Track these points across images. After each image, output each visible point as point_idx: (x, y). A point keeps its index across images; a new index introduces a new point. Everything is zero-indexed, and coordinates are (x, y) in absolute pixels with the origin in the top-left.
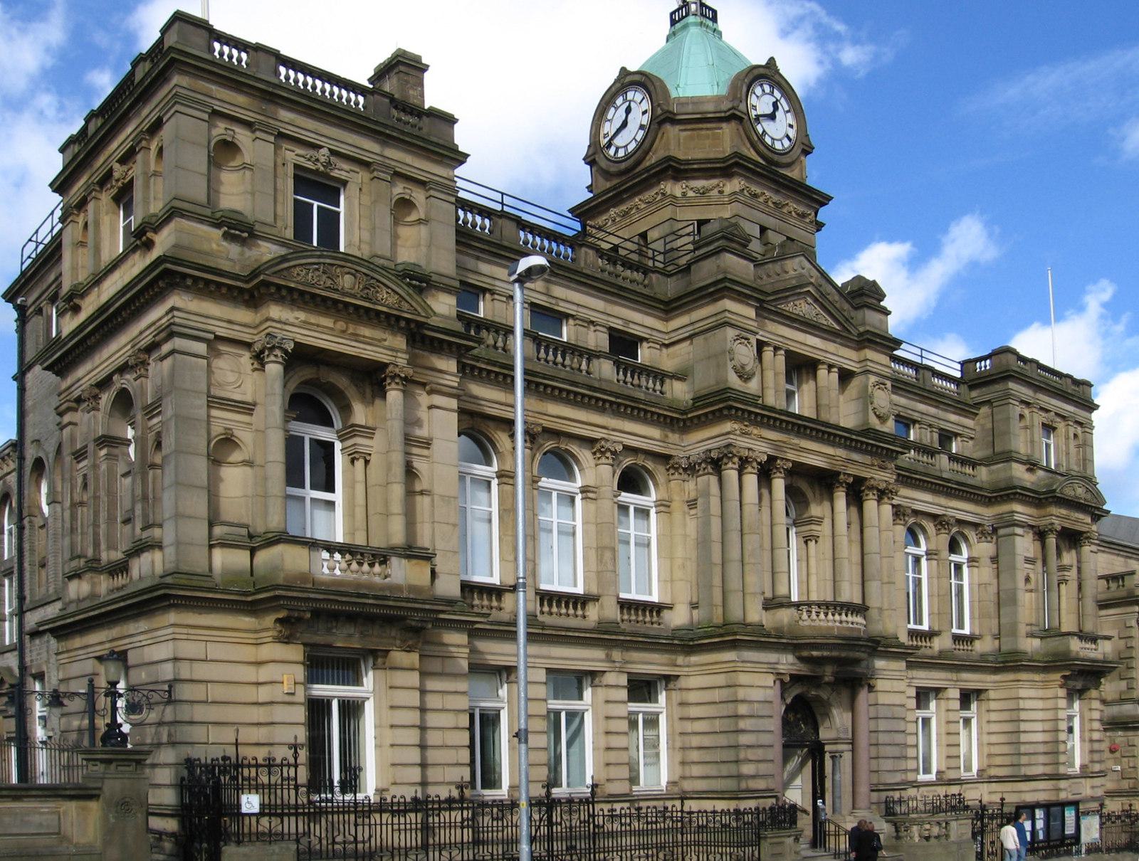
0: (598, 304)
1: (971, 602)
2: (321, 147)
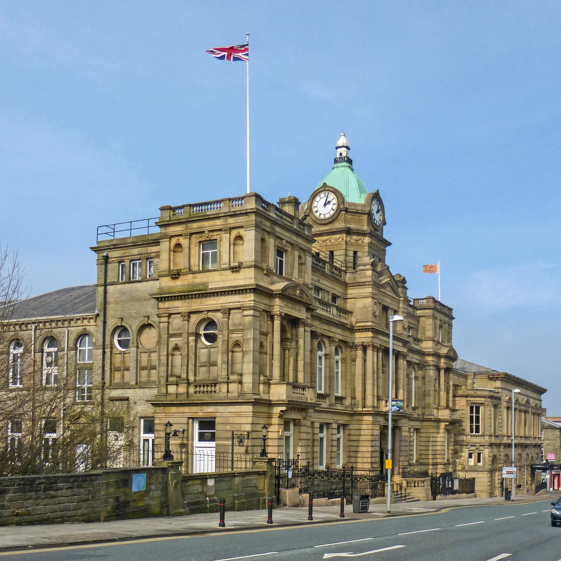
0: (329, 284)
1: (415, 394)
2: (284, 239)
